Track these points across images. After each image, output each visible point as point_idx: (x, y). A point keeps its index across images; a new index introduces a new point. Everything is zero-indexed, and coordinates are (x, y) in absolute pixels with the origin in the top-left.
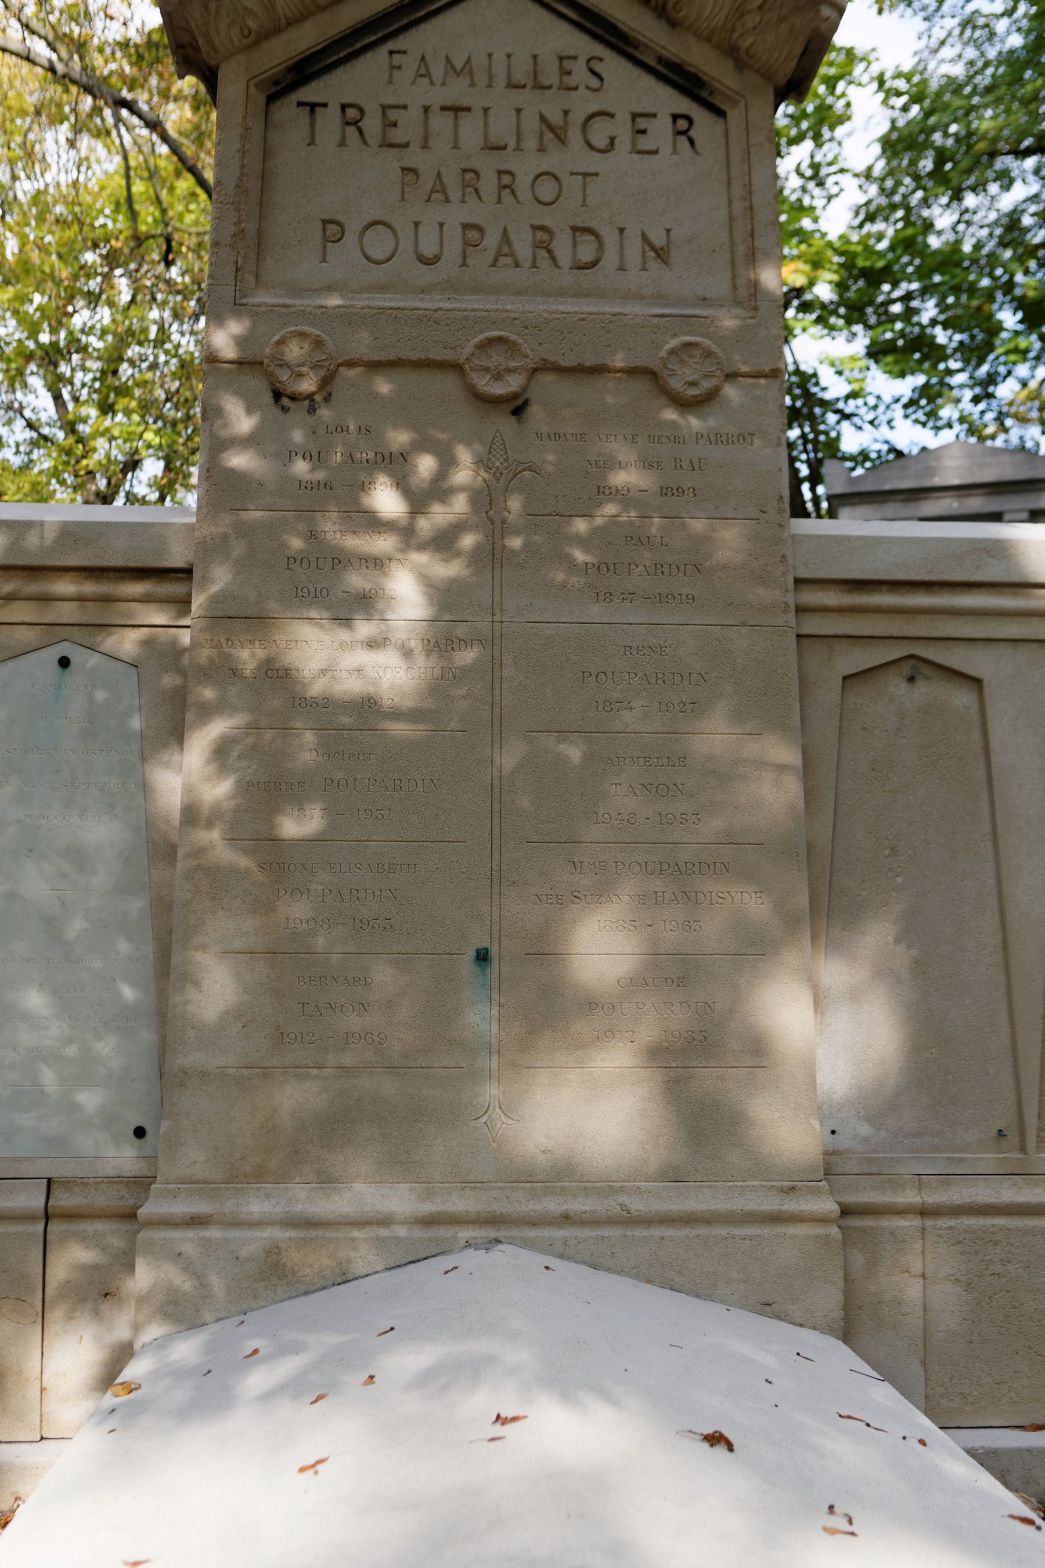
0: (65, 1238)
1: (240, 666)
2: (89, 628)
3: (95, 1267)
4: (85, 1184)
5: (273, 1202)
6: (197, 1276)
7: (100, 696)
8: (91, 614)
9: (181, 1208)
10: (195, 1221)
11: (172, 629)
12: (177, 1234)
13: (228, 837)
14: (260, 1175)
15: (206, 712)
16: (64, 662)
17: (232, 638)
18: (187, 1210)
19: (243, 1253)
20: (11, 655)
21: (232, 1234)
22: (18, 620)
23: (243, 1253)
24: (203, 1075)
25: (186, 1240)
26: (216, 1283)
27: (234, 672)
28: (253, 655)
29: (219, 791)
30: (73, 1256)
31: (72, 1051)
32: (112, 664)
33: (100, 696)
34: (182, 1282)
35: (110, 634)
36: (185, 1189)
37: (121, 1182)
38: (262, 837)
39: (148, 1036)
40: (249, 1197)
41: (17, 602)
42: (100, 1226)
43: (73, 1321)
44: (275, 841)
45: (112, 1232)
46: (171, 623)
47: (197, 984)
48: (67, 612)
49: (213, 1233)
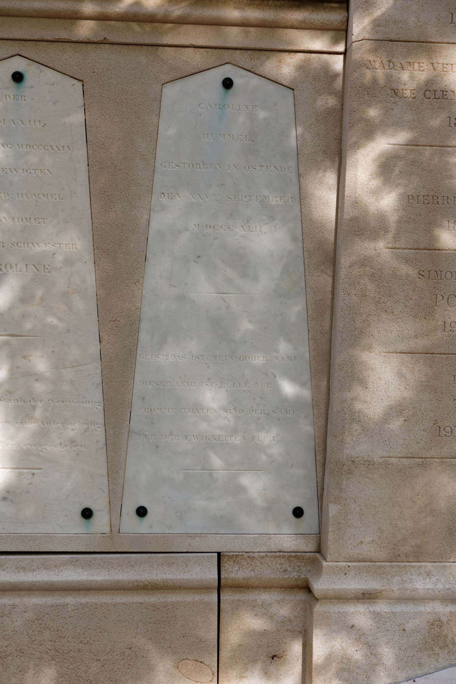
0: (237, 607)
1: (401, 87)
2: (249, 52)
3: (264, 633)
4: (253, 558)
5: (434, 579)
6: (371, 648)
7: (262, 114)
8: (253, 38)
9: (352, 584)
10: (367, 597)
11: (325, 56)
12: (350, 608)
13: (390, 245)
14: (418, 555)
15: (370, 132)
16: (228, 84)
17: (394, 60)
18: (359, 587)
19: (409, 626)
20: (179, 76)
21: (399, 608)
22: (186, 43)
23: (409, 626)
24: (369, 464)
25: (360, 615)
26: (387, 654)
27: (395, 92)
28: (412, 77)
29: (387, 202)
30: (245, 624)
31: (237, 440)
32: (271, 87)
33: (262, 114)
34: (356, 653)
35: (268, 58)
36: (354, 566)
37: (284, 557)
38: (422, 246)
39: (307, 428)
40: (412, 574)
41: (185, 26)
42: (265, 597)
43: (244, 680)
44: (432, 249)
45: (278, 602)
46: (325, 49)
47: (363, 383)
48: (234, 36)
49: (382, 607)
